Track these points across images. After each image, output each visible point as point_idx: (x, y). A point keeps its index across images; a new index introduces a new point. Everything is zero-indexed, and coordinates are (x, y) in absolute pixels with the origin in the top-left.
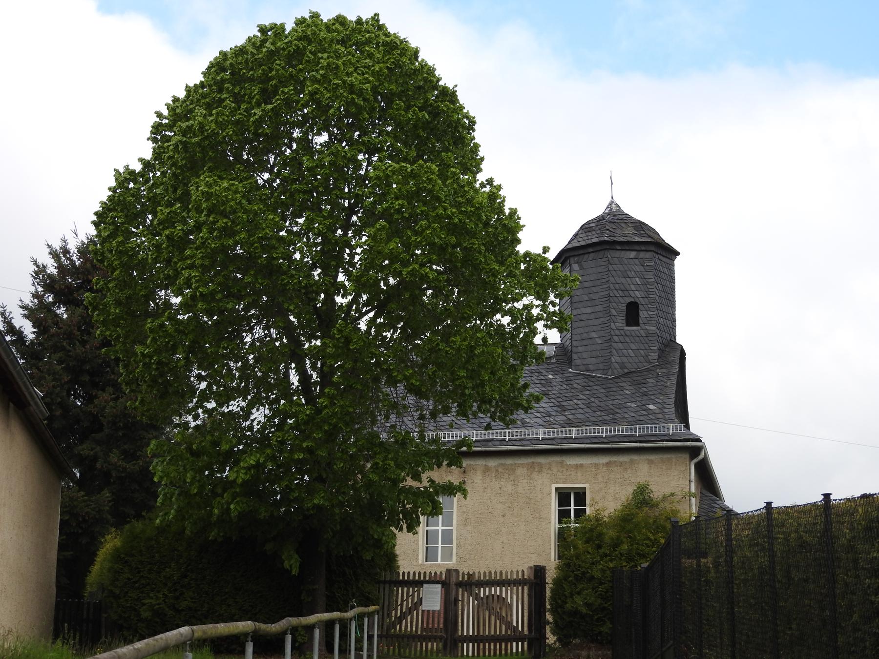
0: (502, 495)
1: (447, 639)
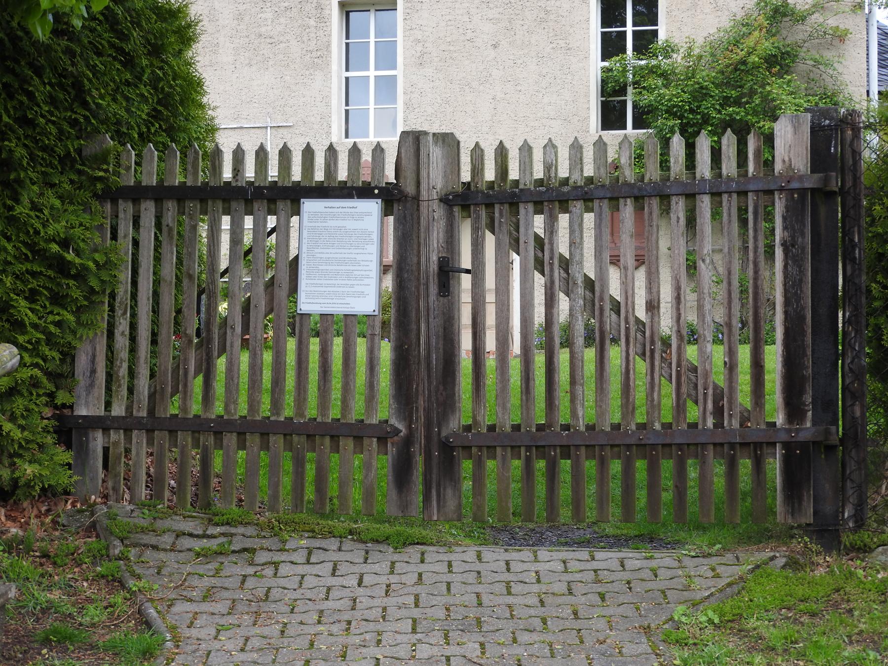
0: (491, 5)
1: (408, 441)
